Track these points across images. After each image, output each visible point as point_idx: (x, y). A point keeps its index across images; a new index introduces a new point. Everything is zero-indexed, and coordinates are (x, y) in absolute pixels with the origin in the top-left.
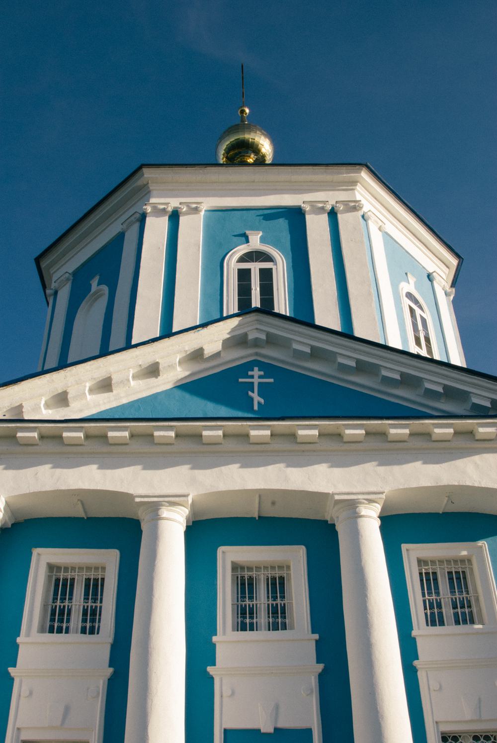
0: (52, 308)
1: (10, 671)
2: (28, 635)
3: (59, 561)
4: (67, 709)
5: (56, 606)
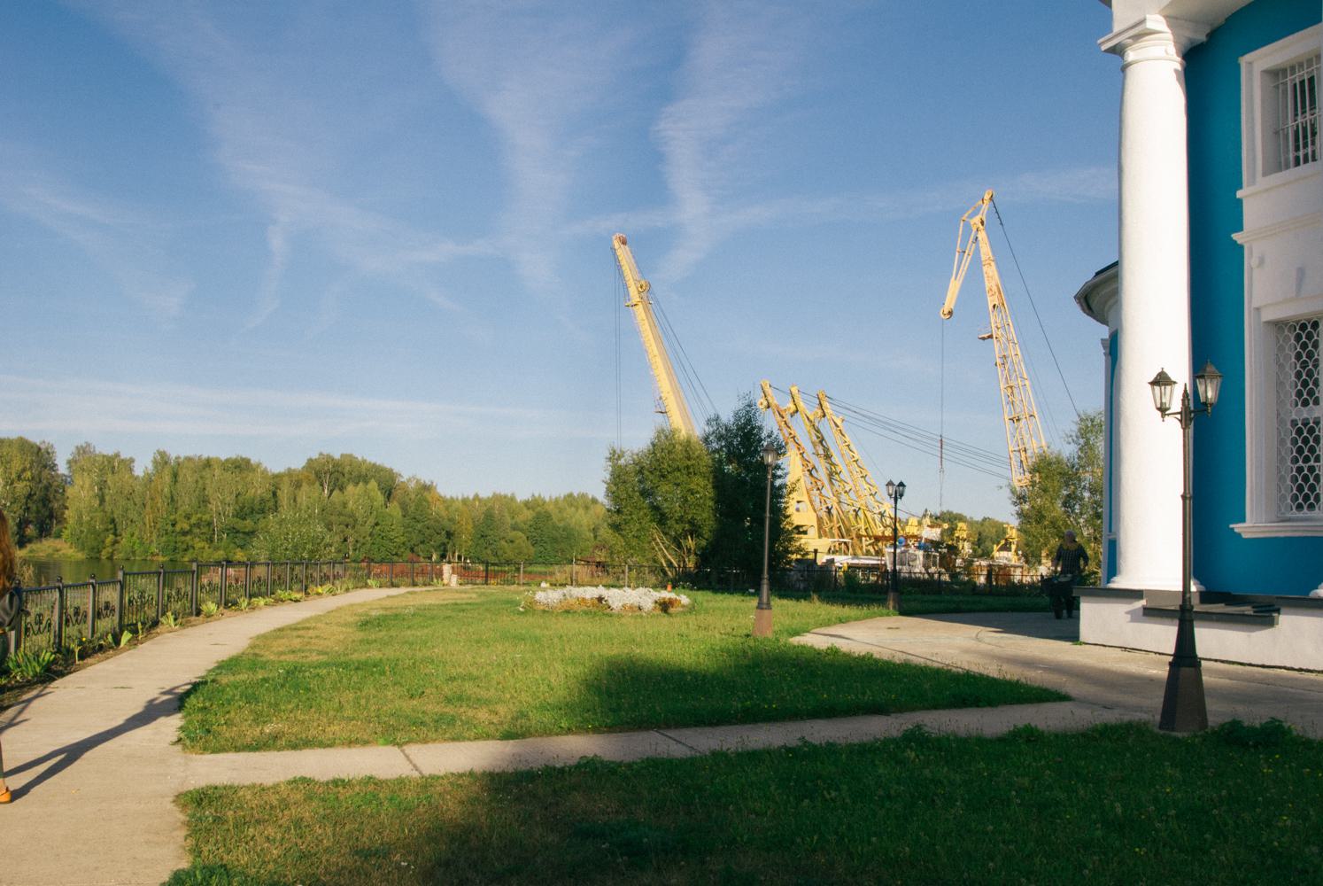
0: (46, 771)
1: (1234, 238)
2: (1253, 182)
3: (1280, 61)
4: (1301, 272)
5: (1297, 126)
